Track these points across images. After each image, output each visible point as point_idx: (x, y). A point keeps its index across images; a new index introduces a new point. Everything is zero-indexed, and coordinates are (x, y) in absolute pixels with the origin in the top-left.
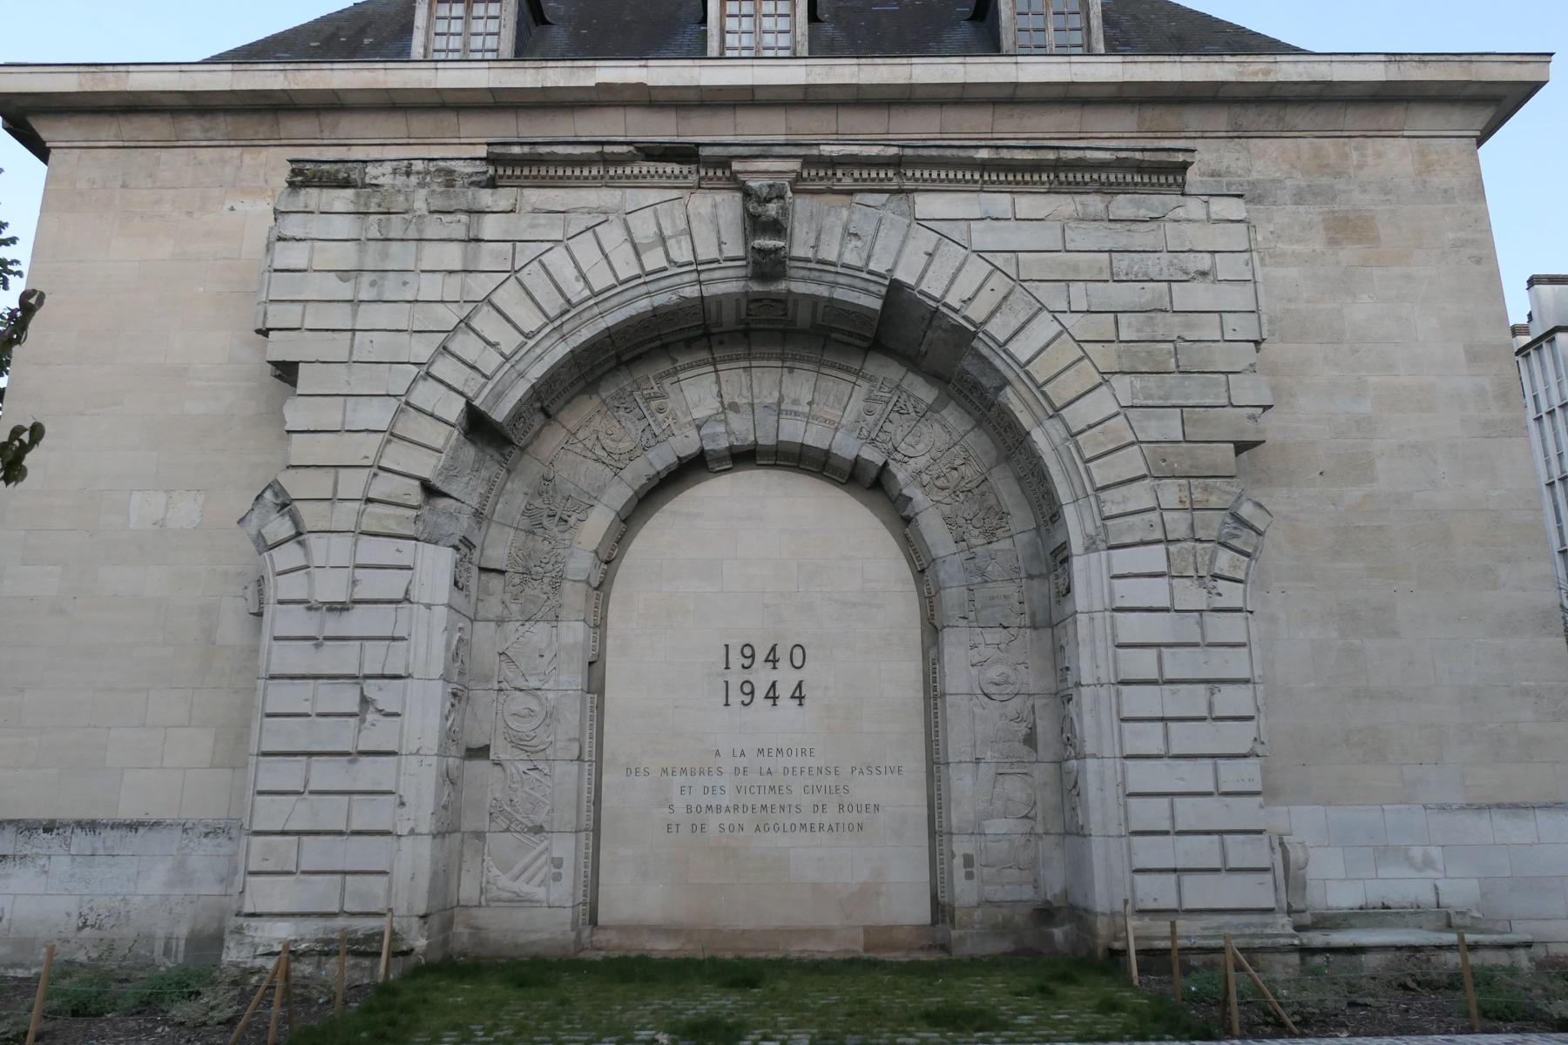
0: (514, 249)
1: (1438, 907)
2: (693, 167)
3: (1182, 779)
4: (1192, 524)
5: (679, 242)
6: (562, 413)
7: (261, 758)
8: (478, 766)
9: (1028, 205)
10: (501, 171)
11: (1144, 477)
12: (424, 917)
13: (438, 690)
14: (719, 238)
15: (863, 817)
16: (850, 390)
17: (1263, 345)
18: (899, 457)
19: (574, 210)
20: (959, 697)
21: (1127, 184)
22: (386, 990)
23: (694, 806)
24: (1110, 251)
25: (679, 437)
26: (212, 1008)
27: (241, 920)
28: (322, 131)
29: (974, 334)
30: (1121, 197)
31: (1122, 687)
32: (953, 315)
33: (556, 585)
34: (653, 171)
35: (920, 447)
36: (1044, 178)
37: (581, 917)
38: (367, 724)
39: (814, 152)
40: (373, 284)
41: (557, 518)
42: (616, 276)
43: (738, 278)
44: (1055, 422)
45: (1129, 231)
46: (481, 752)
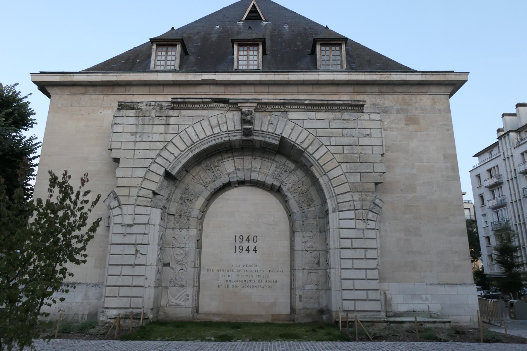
0: (178, 127)
1: (429, 311)
2: (228, 105)
3: (356, 275)
4: (362, 205)
5: (223, 125)
6: (191, 171)
7: (109, 266)
8: (167, 269)
9: (320, 115)
10: (175, 106)
11: (349, 192)
12: (151, 309)
13: (156, 248)
14: (234, 124)
15: (272, 284)
16: (271, 165)
17: (384, 155)
18: (284, 184)
19: (195, 116)
20: (299, 251)
21: (347, 110)
22: (142, 327)
23: (226, 280)
24: (342, 128)
25: (223, 178)
26: (99, 331)
27: (103, 309)
28: (126, 91)
29: (304, 152)
30: (346, 113)
31: (341, 250)
32: (298, 146)
33: (189, 219)
34: (216, 105)
35: (290, 181)
36: (324, 108)
37: (194, 311)
38: (137, 257)
39: (261, 101)
40: (140, 136)
41: (189, 200)
42: (206, 135)
43: (239, 135)
44: (325, 176)
45: (348, 123)
46: (167, 265)
